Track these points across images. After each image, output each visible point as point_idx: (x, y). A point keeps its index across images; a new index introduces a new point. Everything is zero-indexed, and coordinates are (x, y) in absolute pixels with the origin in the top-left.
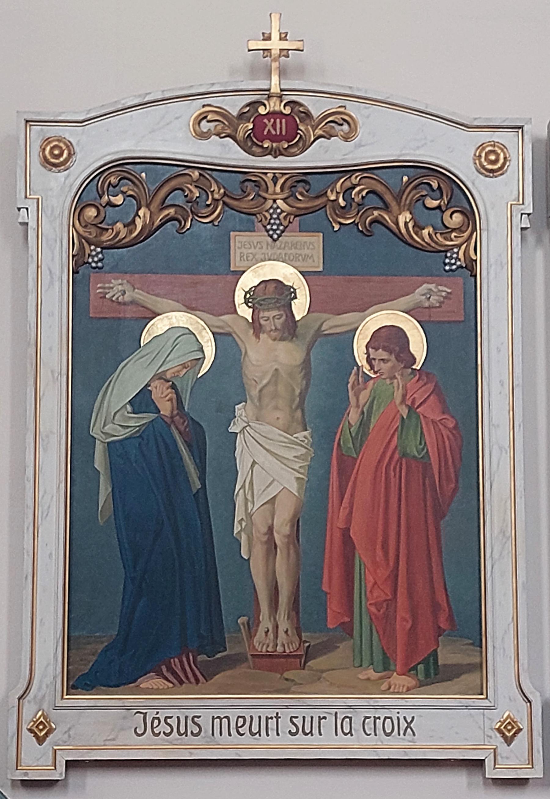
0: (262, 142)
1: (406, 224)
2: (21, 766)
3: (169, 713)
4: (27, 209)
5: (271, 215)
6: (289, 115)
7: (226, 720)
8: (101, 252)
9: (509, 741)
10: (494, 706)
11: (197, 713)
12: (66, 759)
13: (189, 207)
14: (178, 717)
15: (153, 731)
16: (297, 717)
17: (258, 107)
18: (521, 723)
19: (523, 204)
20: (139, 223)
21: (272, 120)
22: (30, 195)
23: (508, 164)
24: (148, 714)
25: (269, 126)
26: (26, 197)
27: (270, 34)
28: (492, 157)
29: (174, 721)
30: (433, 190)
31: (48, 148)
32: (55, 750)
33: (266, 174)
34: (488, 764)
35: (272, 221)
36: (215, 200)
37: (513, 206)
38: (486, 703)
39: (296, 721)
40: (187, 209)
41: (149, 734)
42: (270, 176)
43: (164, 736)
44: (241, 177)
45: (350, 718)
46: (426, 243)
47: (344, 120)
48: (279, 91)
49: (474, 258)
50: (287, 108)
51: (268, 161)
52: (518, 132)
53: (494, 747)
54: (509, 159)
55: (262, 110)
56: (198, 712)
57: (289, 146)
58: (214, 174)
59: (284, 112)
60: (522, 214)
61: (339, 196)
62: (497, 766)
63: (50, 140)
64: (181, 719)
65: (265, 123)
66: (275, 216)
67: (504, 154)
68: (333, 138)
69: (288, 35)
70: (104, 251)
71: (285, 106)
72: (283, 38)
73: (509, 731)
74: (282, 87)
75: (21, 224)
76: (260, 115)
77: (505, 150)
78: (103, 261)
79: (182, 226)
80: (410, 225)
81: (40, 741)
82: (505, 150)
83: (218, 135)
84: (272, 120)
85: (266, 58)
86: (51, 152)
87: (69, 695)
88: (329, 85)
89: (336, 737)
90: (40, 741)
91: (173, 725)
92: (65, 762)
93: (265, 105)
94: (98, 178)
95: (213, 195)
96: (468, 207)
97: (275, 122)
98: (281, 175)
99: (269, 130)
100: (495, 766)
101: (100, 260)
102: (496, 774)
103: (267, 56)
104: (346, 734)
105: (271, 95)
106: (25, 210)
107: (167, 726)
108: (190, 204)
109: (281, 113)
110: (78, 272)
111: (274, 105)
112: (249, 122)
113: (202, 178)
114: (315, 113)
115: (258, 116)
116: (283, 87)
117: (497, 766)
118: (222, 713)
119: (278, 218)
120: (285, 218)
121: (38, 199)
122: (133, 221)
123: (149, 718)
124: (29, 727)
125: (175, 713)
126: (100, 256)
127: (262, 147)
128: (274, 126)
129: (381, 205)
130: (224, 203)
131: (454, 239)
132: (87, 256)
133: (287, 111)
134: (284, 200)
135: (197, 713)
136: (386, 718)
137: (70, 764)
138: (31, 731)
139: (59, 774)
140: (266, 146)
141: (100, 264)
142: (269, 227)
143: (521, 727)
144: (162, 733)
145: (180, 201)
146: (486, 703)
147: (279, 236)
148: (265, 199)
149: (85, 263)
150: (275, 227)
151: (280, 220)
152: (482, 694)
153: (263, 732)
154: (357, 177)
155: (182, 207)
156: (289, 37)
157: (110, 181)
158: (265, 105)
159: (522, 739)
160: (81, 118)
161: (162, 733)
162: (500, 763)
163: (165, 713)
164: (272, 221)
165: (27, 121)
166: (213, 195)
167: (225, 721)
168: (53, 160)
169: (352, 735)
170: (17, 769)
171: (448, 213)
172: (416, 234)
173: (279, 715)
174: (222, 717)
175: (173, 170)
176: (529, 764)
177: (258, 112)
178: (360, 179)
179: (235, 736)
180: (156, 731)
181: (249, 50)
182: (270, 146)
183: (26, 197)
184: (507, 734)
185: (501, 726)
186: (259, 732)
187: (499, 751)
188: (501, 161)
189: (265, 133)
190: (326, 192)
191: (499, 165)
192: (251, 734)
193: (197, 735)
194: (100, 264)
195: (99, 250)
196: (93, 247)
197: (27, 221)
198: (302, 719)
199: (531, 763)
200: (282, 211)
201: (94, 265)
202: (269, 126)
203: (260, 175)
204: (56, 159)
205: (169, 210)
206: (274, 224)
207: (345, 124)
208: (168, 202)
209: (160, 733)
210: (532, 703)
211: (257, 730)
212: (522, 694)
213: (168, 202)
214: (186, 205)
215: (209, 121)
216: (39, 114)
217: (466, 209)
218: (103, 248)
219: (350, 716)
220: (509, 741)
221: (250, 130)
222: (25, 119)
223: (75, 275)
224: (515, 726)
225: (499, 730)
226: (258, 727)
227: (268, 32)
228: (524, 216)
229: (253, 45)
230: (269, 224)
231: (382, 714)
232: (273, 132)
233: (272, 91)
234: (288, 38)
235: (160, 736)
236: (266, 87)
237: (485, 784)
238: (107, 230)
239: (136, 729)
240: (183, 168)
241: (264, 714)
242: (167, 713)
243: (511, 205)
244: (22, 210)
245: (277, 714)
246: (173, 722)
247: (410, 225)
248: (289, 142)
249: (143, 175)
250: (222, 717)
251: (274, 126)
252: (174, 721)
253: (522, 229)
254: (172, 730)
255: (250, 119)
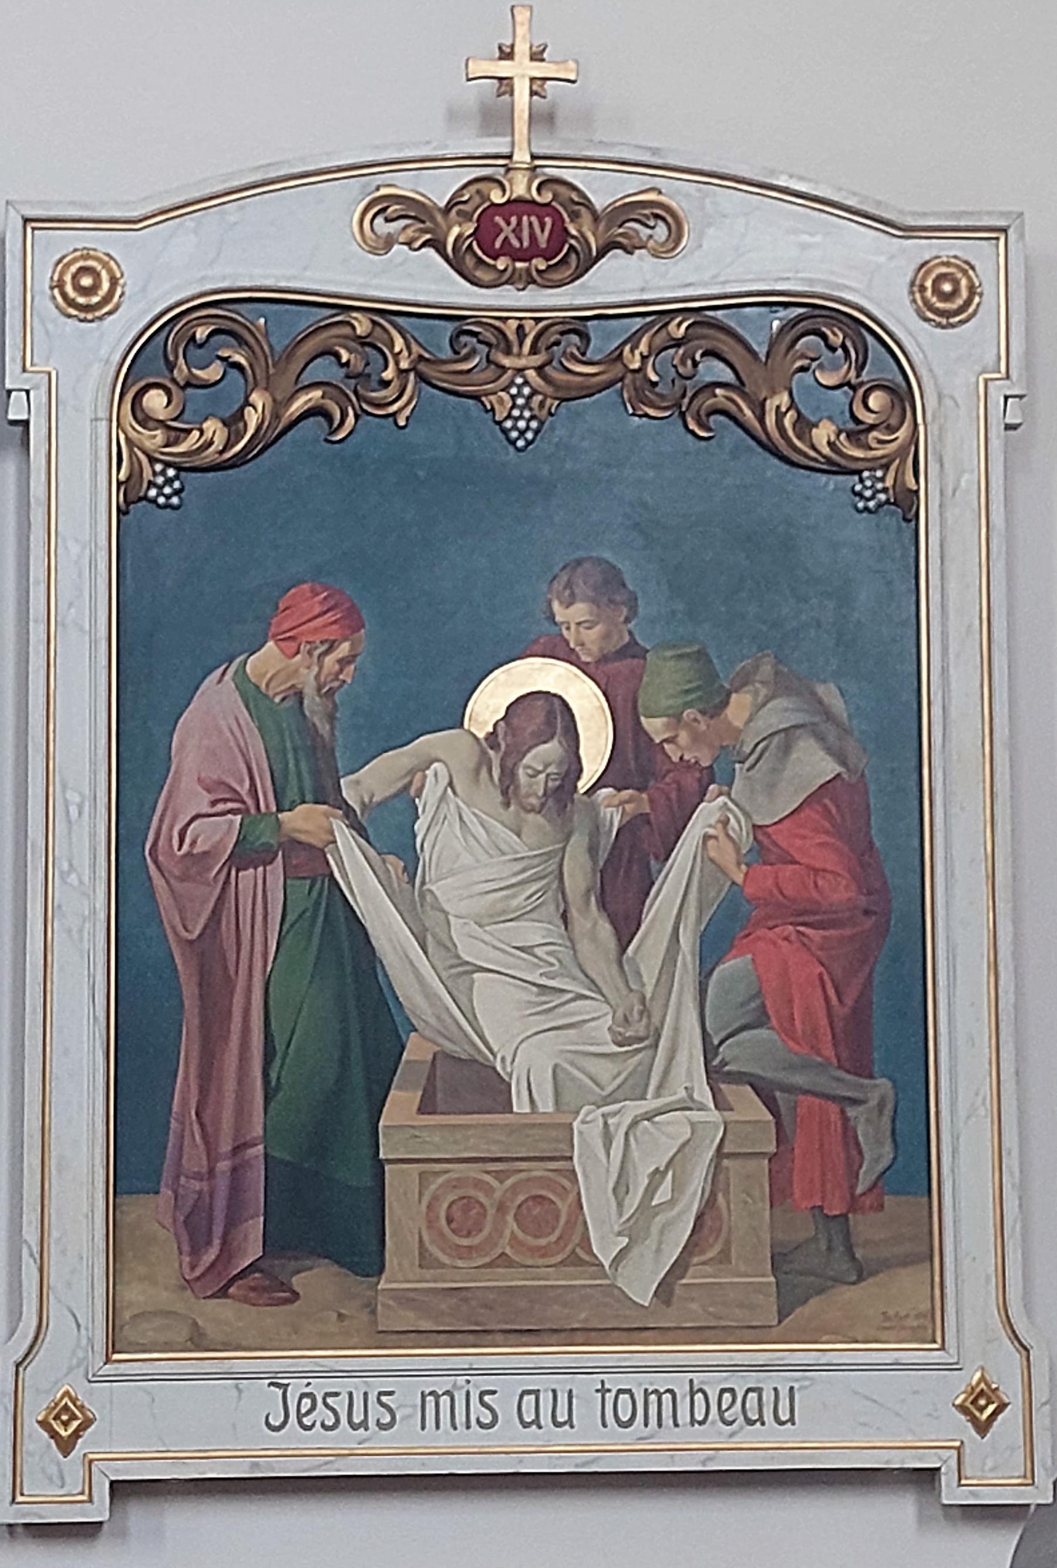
0: (495, 258)
1: (780, 416)
2: (966, 1478)
3: (332, 1384)
4: (28, 392)
5: (513, 397)
6: (548, 205)
7: (668, 1396)
8: (177, 477)
9: (983, 1428)
10: (957, 1363)
11: (387, 1384)
12: (113, 1478)
13: (352, 387)
14: (351, 1395)
15: (300, 1422)
16: (336, 1394)
17: (491, 190)
18: (1005, 1394)
19: (1008, 377)
20: (252, 419)
21: (514, 220)
22: (32, 365)
23: (977, 299)
24: (290, 1388)
25: (507, 231)
26: (24, 370)
27: (512, 46)
28: (947, 287)
29: (341, 1402)
30: (833, 349)
31: (68, 278)
32: (91, 1461)
33: (504, 320)
34: (947, 1480)
35: (516, 413)
36: (402, 373)
37: (990, 383)
38: (936, 1357)
39: (492, 1400)
40: (348, 392)
41: (293, 1425)
42: (513, 324)
43: (322, 1431)
44: (450, 327)
45: (759, 1391)
46: (824, 457)
47: (657, 216)
48: (528, 159)
49: (911, 484)
50: (543, 192)
51: (507, 296)
52: (997, 239)
53: (957, 1444)
54: (979, 290)
55: (497, 197)
56: (534, 1382)
57: (549, 267)
58: (400, 320)
59: (538, 199)
60: (1006, 398)
61: (647, 363)
62: (963, 1482)
63: (65, 261)
64: (781, 1396)
65: (497, 225)
66: (520, 401)
67: (110, 271)
68: (637, 252)
69: (547, 50)
70: (183, 474)
71: (539, 189)
72: (506, 54)
73: (982, 1409)
74: (535, 150)
75: (14, 423)
76: (493, 205)
77: (971, 272)
78: (183, 495)
79: (336, 422)
80: (788, 422)
81: (66, 1446)
82: (971, 272)
83: (408, 244)
84: (514, 220)
85: (503, 97)
86: (937, 290)
87: (119, 1352)
88: (613, 145)
89: (605, 1430)
90: (66, 1446)
91: (338, 1410)
92: (107, 1485)
93: (504, 191)
94: (167, 329)
95: (397, 363)
96: (904, 384)
97: (519, 223)
98: (532, 322)
99: (506, 238)
100: (960, 1480)
101: (177, 493)
102: (102, 1501)
103: (504, 93)
104: (526, 1425)
105: (511, 166)
106: (24, 394)
107: (483, 1409)
108: (353, 381)
109: (533, 202)
110: (126, 513)
111: (520, 186)
112: (471, 220)
113: (378, 329)
114: (600, 202)
115: (488, 207)
116: (536, 151)
117: (963, 1482)
118: (442, 1384)
119: (527, 405)
120: (542, 404)
121: (49, 374)
122: (239, 415)
123: (293, 1396)
124: (40, 1418)
125: (344, 1386)
126: (177, 485)
127: (494, 267)
128: (517, 231)
129: (728, 376)
130: (421, 378)
131: (874, 445)
132: (145, 485)
133: (547, 197)
134: (539, 369)
135: (387, 1384)
136: (620, 1391)
137: (120, 1490)
138: (44, 1424)
139: (99, 1511)
140: (501, 267)
141: (175, 500)
142: (509, 424)
143: (1007, 1400)
144: (318, 1424)
145: (336, 375)
146: (936, 1357)
147: (529, 443)
148: (504, 369)
149: (140, 499)
150: (522, 424)
151: (531, 409)
152: (934, 1342)
153: (768, 1416)
154: (679, 325)
155: (336, 387)
156: (549, 55)
157: (194, 334)
158: (504, 191)
159: (1009, 1422)
160: (135, 214)
161: (318, 1424)
162: (969, 1475)
163: (324, 1385)
164: (516, 413)
165: (26, 220)
166: (397, 363)
167: (667, 1398)
168: (81, 300)
169: (763, 1424)
170: (960, 1485)
171: (861, 391)
172: (799, 438)
173: (607, 1386)
174: (662, 1390)
175: (637, 323)
176: (82, 1493)
177: (489, 199)
178: (687, 328)
179: (446, 1432)
180: (307, 1421)
181: (469, 80)
182: (510, 269)
183: (24, 370)
184: (977, 1414)
185: (965, 1400)
186: (536, 1422)
187: (967, 1450)
188: (106, 286)
189: (498, 245)
190: (621, 354)
191: (960, 302)
192: (352, 1427)
193: (491, 1425)
194: (175, 500)
195: (171, 472)
196: (158, 467)
197: (25, 417)
198: (347, 1396)
199: (87, 1491)
200: (534, 392)
201: (161, 500)
202: (507, 231)
203: (497, 323)
204: (96, 294)
205: (307, 394)
206: (521, 417)
207: (661, 223)
208: (306, 379)
209: (313, 1425)
210: (1031, 1352)
211: (533, 1417)
212: (41, 1336)
213: (306, 379)
214: (345, 384)
215: (387, 220)
216: (85, 206)
217: (898, 386)
218: (179, 468)
219: (536, 1388)
220: (983, 1428)
221: (469, 237)
222: (23, 217)
223: (123, 518)
224: (994, 1398)
225: (962, 1408)
226: (533, 1410)
227: (509, 43)
228: (1010, 400)
229: (478, 68)
230: (509, 416)
231: (614, 1382)
232: (516, 243)
233: (516, 158)
234: (545, 55)
235: (314, 1430)
236: (505, 150)
237: (946, 1516)
238: (189, 432)
239: (267, 1418)
240: (334, 312)
241: (640, 1384)
242: (382, 1384)
243: (986, 381)
244: (14, 394)
245: (603, 1382)
246: (340, 1404)
247: (788, 422)
248: (548, 260)
249: (262, 321)
250: (662, 1390)
251: (517, 231)
252: (342, 1401)
253: (1008, 427)
254: (495, 1418)
255: (472, 216)
